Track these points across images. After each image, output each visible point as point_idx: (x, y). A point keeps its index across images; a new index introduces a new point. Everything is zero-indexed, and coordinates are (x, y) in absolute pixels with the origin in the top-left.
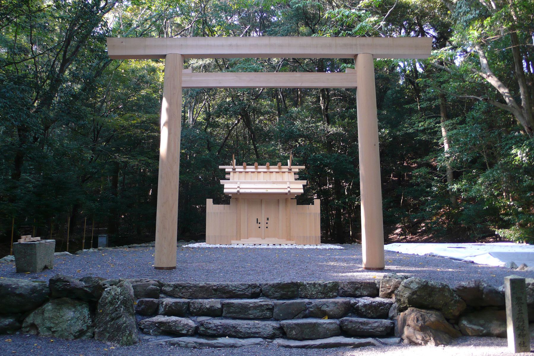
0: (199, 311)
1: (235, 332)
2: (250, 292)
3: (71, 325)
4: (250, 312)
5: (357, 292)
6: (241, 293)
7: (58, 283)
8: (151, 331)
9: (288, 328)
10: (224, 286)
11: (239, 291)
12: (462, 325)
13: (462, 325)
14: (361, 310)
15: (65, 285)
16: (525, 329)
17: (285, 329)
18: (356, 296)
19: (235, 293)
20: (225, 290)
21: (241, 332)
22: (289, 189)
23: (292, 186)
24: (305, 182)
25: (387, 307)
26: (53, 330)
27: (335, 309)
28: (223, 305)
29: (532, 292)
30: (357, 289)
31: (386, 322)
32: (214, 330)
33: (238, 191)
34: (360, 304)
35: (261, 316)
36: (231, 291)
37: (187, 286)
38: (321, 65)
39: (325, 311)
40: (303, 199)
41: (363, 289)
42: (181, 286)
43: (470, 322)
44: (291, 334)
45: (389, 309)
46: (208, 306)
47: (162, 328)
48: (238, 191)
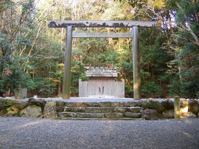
18: (129, 106)
22: (112, 75)
30: (130, 104)
31: (139, 114)
43: (165, 112)
46: (80, 109)
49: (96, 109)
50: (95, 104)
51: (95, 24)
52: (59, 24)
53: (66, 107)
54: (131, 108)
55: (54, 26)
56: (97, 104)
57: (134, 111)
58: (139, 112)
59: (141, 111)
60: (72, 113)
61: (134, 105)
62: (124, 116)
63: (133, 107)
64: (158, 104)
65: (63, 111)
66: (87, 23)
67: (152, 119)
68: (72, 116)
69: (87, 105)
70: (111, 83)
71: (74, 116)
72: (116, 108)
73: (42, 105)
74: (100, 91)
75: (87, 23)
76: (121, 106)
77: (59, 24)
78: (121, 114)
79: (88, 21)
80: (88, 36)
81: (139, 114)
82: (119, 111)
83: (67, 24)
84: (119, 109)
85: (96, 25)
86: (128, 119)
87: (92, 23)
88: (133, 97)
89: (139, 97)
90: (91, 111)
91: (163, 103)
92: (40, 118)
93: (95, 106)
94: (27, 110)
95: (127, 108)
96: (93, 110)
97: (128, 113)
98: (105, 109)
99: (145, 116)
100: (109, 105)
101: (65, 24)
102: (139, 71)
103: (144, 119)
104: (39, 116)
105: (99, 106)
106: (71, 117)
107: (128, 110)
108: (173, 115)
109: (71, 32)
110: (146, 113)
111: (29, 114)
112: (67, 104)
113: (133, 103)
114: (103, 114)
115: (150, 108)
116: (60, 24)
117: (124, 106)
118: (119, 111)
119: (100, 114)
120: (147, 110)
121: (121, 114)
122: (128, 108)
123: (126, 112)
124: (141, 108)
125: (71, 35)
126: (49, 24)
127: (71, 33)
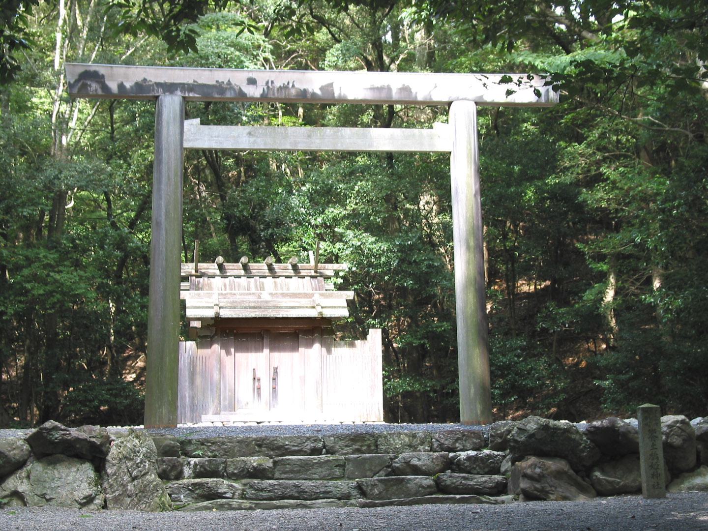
0: (243, 471)
1: (299, 492)
2: (309, 447)
3: (74, 490)
4: (313, 471)
5: (457, 445)
6: (296, 448)
7: (53, 433)
8: (182, 497)
9: (368, 486)
10: (272, 439)
11: (294, 446)
12: (594, 478)
13: (594, 478)
14: (463, 465)
15: (64, 434)
16: (659, 467)
17: (364, 488)
18: (453, 450)
19: (288, 449)
20: (274, 445)
21: (306, 492)
22: (319, 309)
23: (325, 302)
24: (350, 294)
25: (499, 460)
26: (48, 497)
27: (428, 462)
28: (275, 463)
29: (680, 431)
30: (457, 440)
31: (498, 478)
32: (270, 491)
33: (217, 314)
34: (462, 457)
35: (329, 475)
36: (282, 447)
37: (219, 442)
38: (386, 115)
39: (416, 465)
40: (350, 330)
41: (465, 441)
42: (208, 442)
43: (603, 472)
44: (373, 494)
45: (501, 462)
46: (255, 464)
47: (197, 492)
48: (217, 314)
49: (320, 464)
50: (309, 445)
51: (285, 87)
52: (121, 86)
53: (193, 461)
54: (463, 455)
55: (100, 92)
56: (320, 445)
57: (475, 469)
58: (498, 472)
59: (506, 465)
60: (226, 482)
61: (475, 443)
62: (440, 488)
63: (472, 453)
64: (573, 436)
65: (179, 476)
66: (252, 82)
67: (552, 497)
68: (225, 493)
69: (279, 448)
70: (312, 354)
71: (234, 494)
72: (400, 456)
73: (95, 456)
74: (259, 389)
75: (252, 82)
76: (421, 447)
77: (121, 86)
78: (428, 481)
79: (254, 75)
80: (254, 142)
81: (498, 478)
82: (416, 470)
83: (159, 85)
84: (415, 462)
85: (293, 92)
86: (458, 496)
87: (272, 82)
88: (456, 418)
89: (483, 412)
90: (298, 472)
91: (592, 433)
92: (92, 507)
93: (315, 451)
94: (28, 477)
95: (446, 457)
96: (305, 467)
97: (449, 478)
98: (359, 463)
99: (524, 484)
100: (369, 446)
101: (150, 85)
102: (188, 191)
103: (521, 496)
104: (89, 500)
105: (327, 453)
106: (221, 496)
107: (451, 465)
108: (634, 481)
109: (178, 124)
110: (529, 471)
111: (43, 496)
112: (190, 448)
113: (464, 436)
114: (354, 483)
115: (541, 454)
116: (128, 85)
117: (431, 450)
118: (416, 470)
119: (339, 482)
120: (532, 460)
121: (428, 481)
122: (451, 454)
123: (443, 470)
124: (504, 457)
125: (178, 137)
126: (72, 82)
127: (178, 131)
